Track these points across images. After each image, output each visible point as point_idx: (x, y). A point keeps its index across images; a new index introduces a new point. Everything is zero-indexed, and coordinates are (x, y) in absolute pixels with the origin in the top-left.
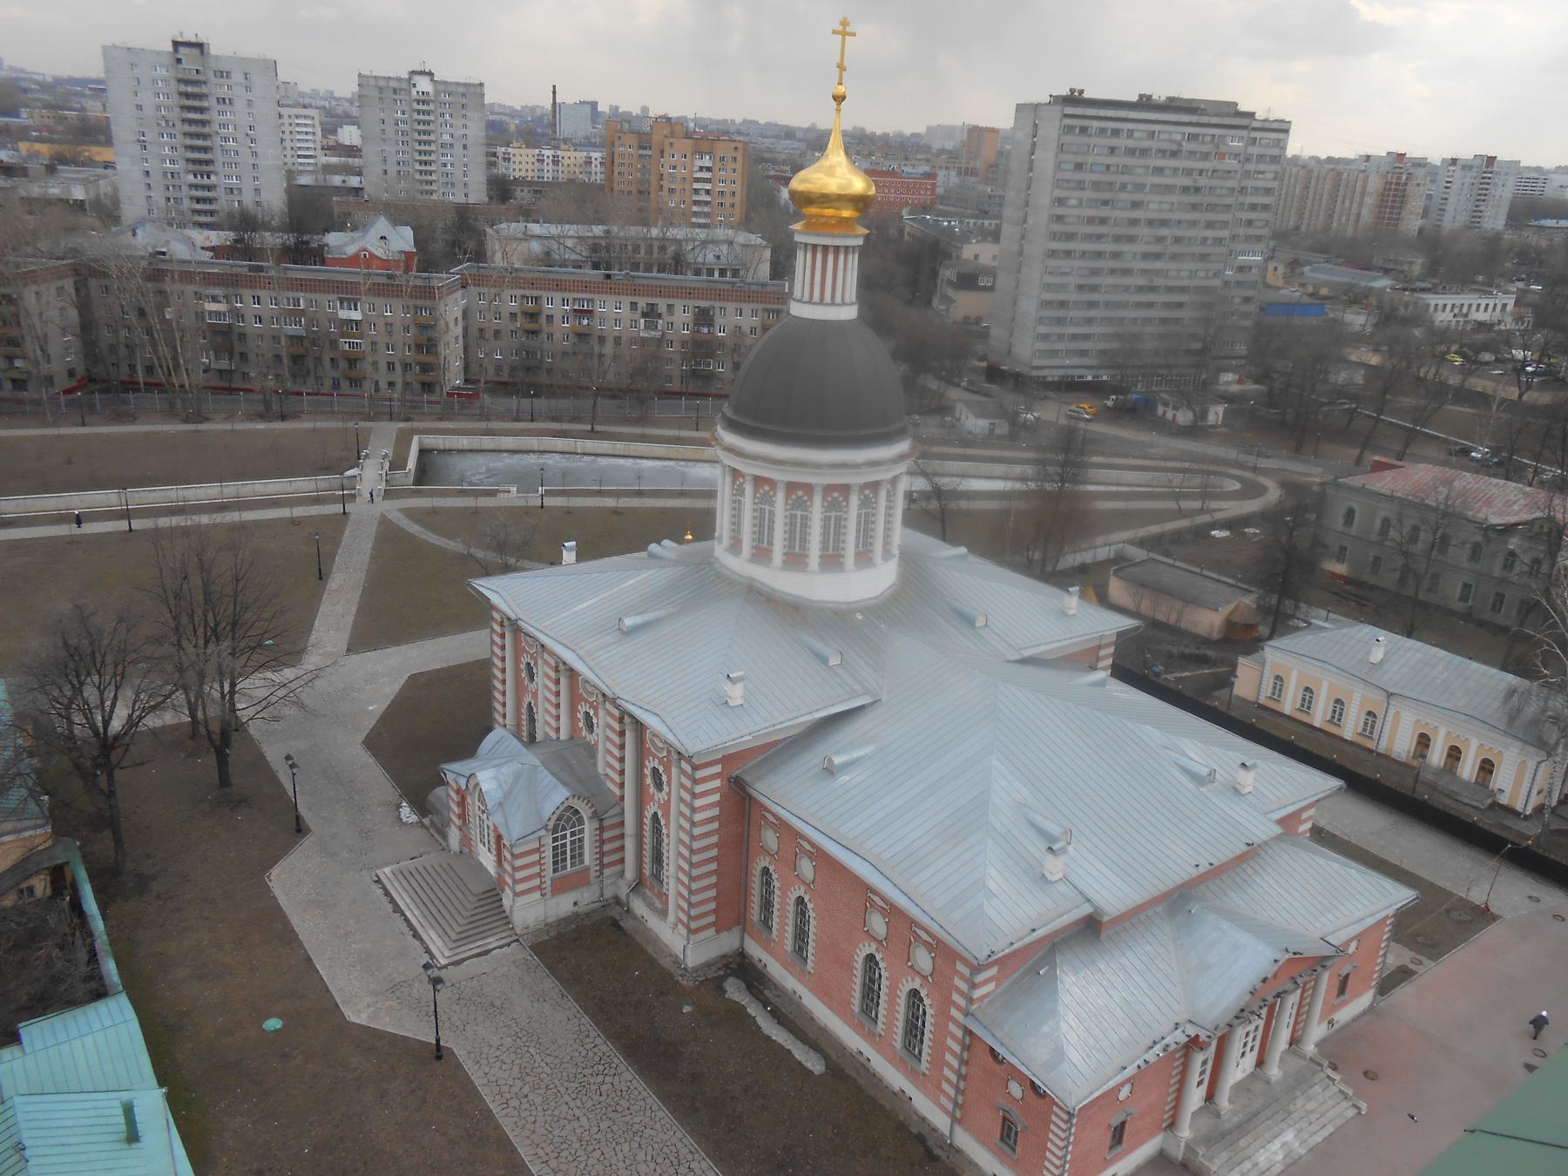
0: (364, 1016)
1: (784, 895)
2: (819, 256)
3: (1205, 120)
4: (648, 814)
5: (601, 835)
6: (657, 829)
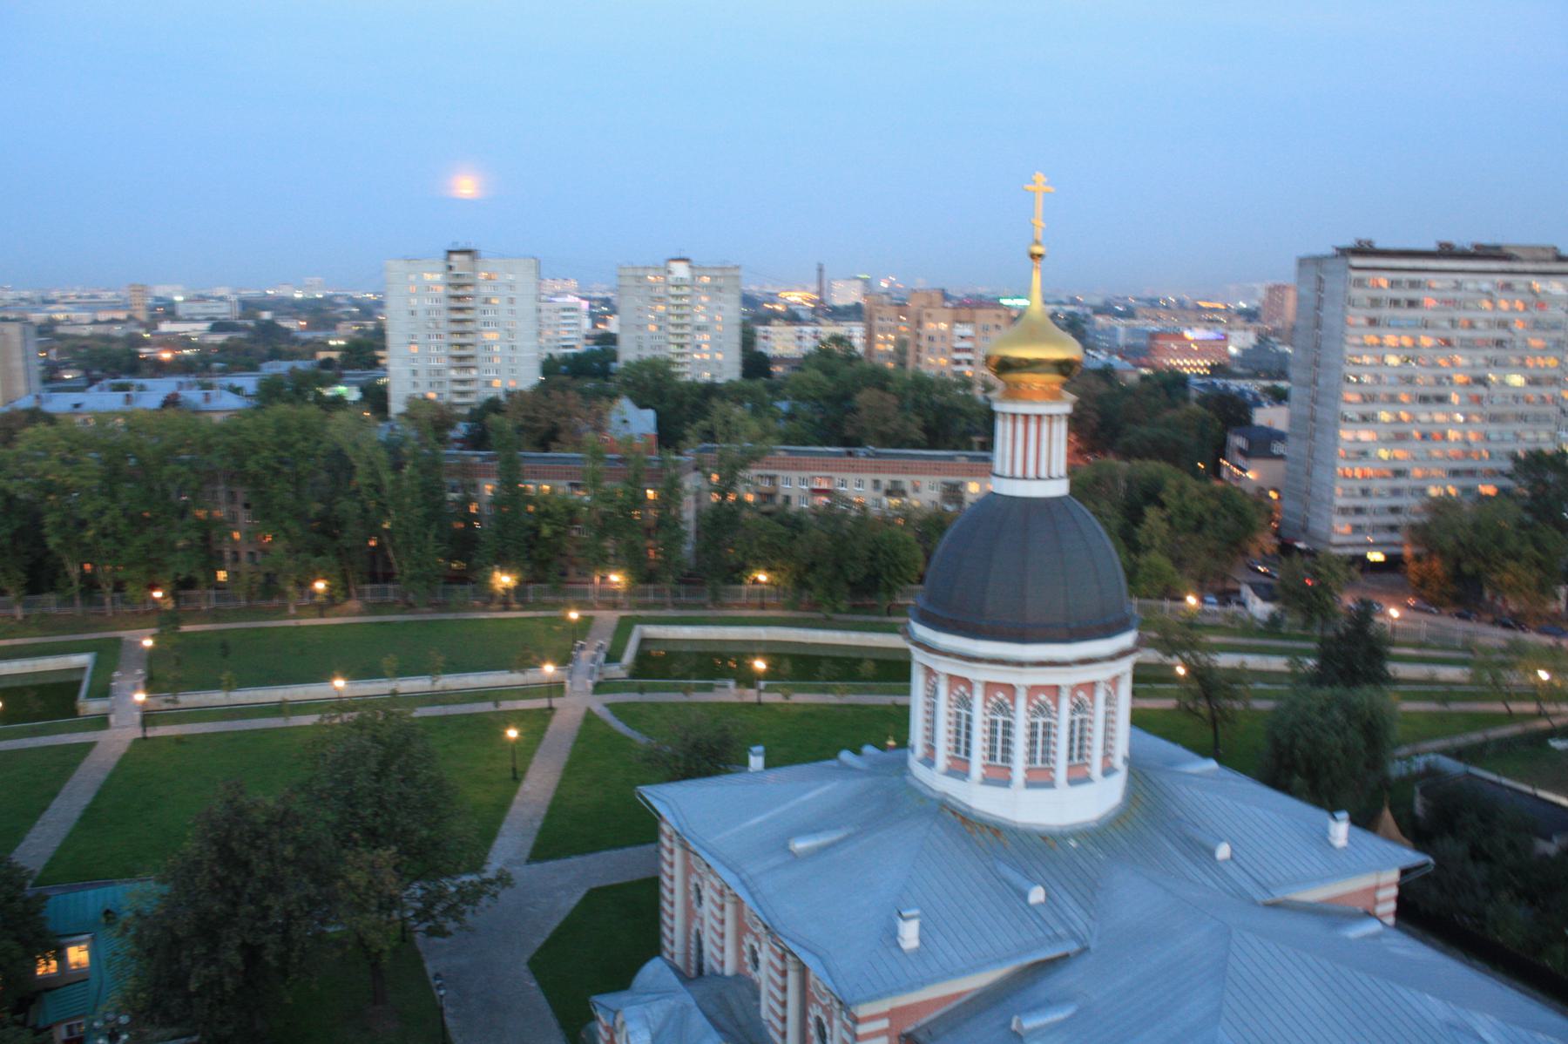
3: (1517, 266)
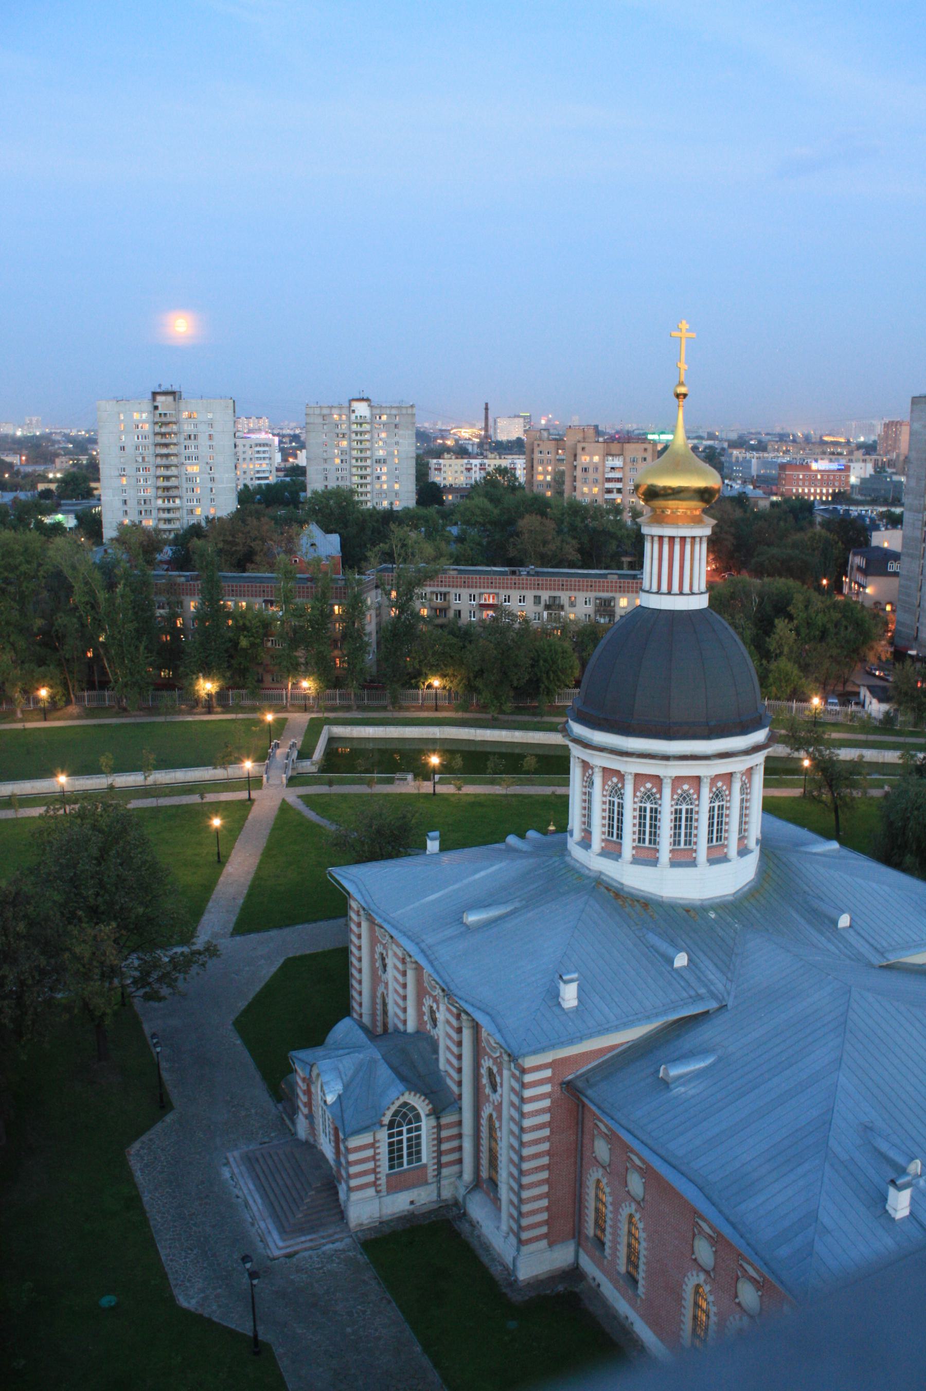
0: (194, 1301)
1: (616, 1212)
2: (677, 548)
4: (485, 1115)
5: (439, 1133)
6: (492, 1129)
